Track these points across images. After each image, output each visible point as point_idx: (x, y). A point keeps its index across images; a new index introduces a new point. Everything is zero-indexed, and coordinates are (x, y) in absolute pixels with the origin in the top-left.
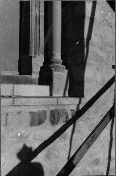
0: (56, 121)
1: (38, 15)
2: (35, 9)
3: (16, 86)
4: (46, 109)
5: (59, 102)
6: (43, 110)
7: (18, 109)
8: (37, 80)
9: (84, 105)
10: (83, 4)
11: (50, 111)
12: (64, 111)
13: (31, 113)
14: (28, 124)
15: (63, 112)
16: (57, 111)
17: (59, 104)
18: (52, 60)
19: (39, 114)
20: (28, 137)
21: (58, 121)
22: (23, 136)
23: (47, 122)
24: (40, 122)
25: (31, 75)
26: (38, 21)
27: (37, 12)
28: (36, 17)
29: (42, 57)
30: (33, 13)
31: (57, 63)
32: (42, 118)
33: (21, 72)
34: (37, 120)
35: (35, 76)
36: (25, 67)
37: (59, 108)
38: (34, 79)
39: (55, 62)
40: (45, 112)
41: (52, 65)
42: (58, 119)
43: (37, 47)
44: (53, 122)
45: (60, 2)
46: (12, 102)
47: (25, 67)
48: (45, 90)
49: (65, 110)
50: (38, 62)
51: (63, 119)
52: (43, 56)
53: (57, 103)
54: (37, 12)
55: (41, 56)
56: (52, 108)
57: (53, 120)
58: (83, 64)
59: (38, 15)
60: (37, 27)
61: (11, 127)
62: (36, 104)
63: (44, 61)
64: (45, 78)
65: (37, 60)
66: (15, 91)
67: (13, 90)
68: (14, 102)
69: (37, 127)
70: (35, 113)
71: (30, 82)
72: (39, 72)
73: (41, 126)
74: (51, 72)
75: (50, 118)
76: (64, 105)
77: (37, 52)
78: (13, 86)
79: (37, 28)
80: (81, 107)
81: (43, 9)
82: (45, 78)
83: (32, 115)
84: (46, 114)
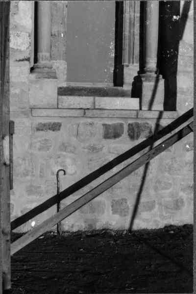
0: (136, 135)
1: (132, 17)
2: (129, 10)
3: (97, 98)
4: (123, 122)
5: (139, 115)
6: (119, 123)
7: (89, 120)
8: (130, 93)
9: (174, 120)
10: (179, 3)
11: (128, 124)
12: (146, 125)
13: (104, 125)
14: (102, 137)
15: (146, 126)
16: (138, 125)
17: (139, 117)
18: (145, 69)
19: (115, 127)
20: (101, 149)
21: (138, 137)
22: (96, 148)
23: (125, 135)
24: (116, 135)
25: (122, 86)
26: (132, 25)
27: (153, 9)
28: (130, 19)
29: (136, 66)
30: (126, 15)
31: (151, 72)
32: (119, 131)
33: (116, 84)
34: (112, 133)
35: (127, 87)
36: (118, 79)
37: (139, 122)
38: (127, 91)
39: (148, 71)
40: (121, 125)
41: (144, 75)
42: (139, 133)
43: (131, 54)
44: (132, 137)
45: (139, 2)
46: (83, 113)
47: (118, 79)
48: (134, 103)
49: (147, 124)
50: (131, 71)
51: (145, 134)
52: (138, 64)
53: (137, 116)
54: (131, 13)
55: (135, 64)
56: (130, 122)
57: (132, 134)
58: (175, 73)
59: (132, 17)
60: (132, 31)
61: (82, 137)
62: (110, 116)
63: (139, 70)
64: (137, 92)
65: (129, 69)
66: (96, 103)
67: (94, 103)
68: (85, 114)
69: (112, 141)
70: (109, 125)
71: (123, 95)
72: (132, 82)
73: (117, 139)
74: (141, 82)
75: (128, 131)
76: (146, 118)
77: (131, 60)
78: (94, 98)
79: (131, 32)
80: (165, 123)
81: (139, 9)
82: (137, 92)
83: (106, 128)
84: (123, 128)
